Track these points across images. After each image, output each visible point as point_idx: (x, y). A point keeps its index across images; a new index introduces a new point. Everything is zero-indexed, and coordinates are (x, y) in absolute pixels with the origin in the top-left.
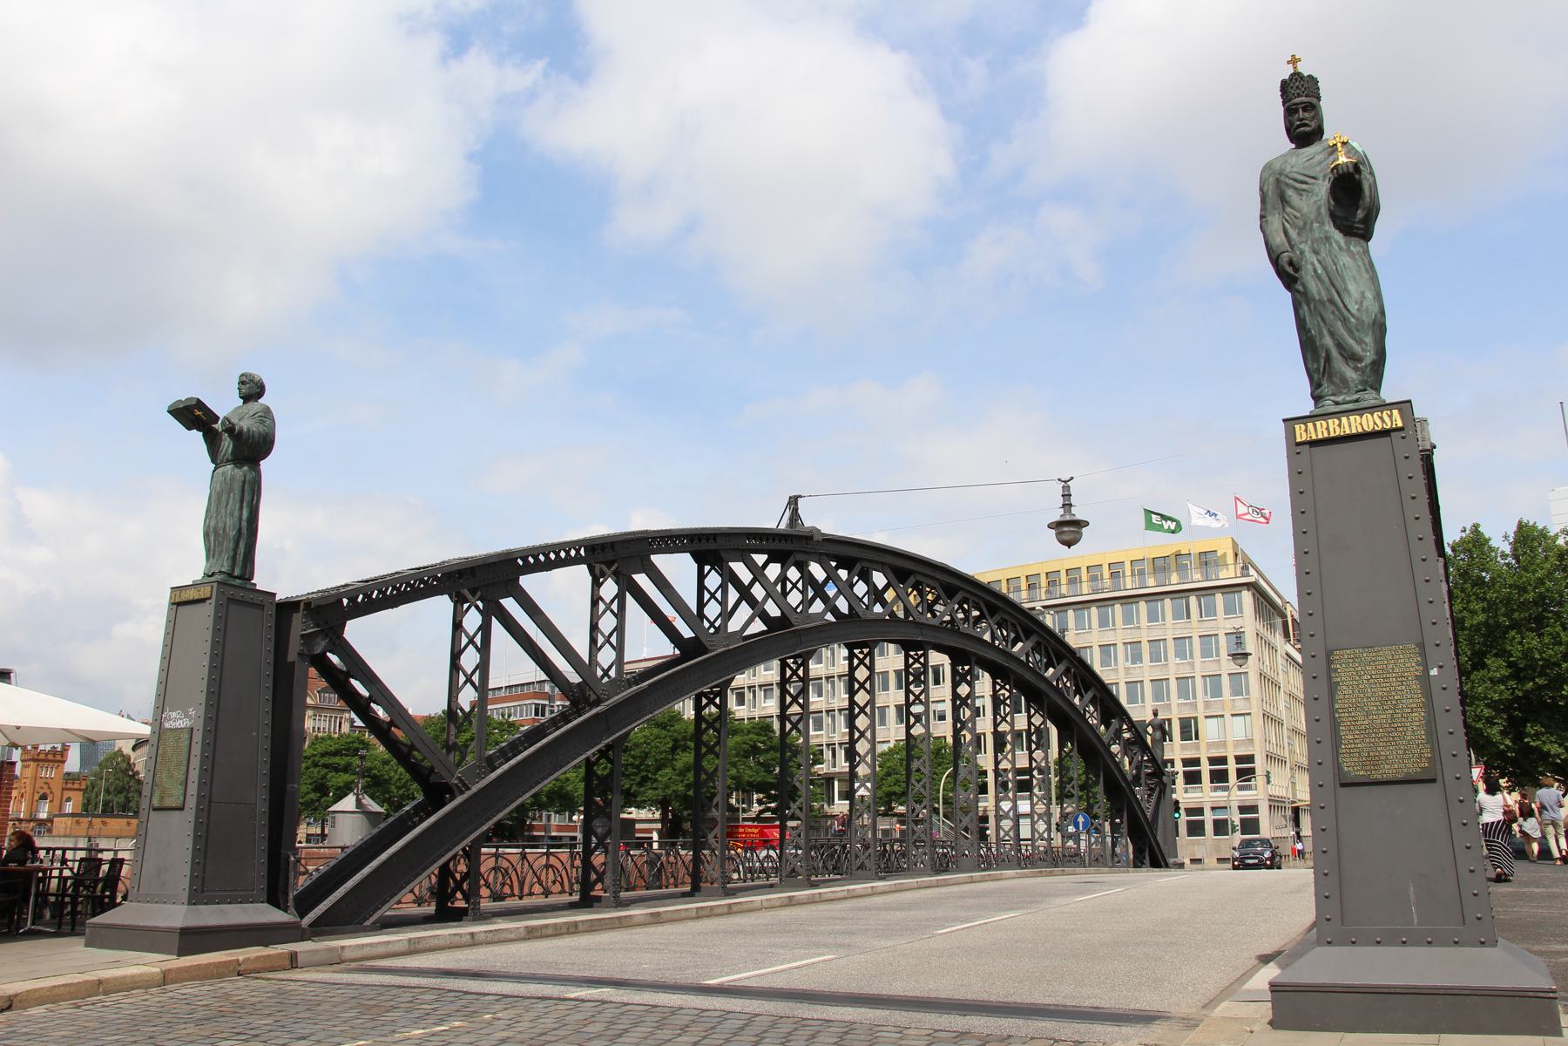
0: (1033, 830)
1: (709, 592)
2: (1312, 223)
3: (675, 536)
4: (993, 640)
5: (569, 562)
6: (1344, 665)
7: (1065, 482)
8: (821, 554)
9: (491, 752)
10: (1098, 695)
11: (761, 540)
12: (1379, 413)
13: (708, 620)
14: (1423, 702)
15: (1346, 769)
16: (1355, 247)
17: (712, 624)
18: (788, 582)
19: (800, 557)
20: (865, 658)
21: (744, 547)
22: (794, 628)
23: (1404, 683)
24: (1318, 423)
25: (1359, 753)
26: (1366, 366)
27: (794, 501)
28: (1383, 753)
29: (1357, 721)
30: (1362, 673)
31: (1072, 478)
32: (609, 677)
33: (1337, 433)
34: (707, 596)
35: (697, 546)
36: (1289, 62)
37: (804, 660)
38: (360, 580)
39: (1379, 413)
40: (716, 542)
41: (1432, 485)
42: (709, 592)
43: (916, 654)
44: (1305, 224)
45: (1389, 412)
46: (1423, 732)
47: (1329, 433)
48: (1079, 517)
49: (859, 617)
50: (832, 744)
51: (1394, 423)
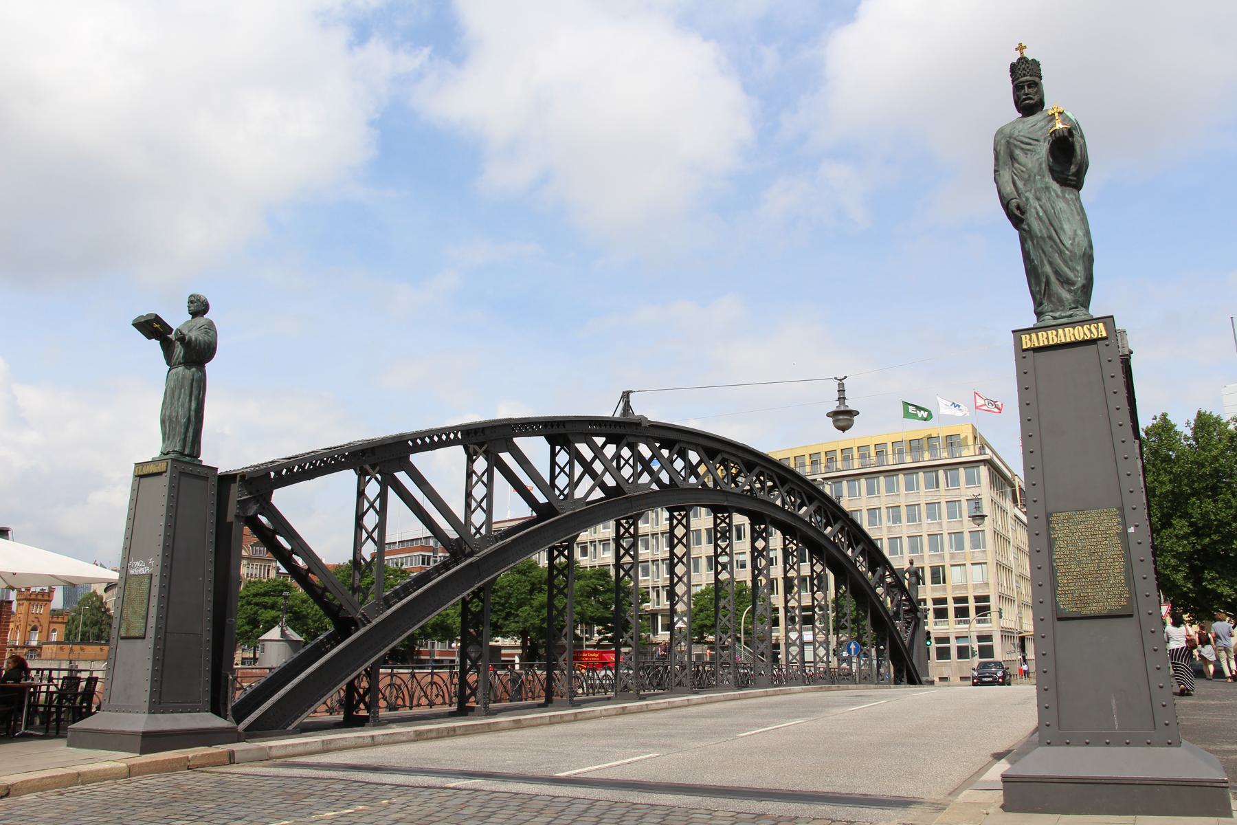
0: (815, 655)
1: (559, 467)
2: (1035, 176)
3: (533, 423)
4: (783, 505)
5: (449, 443)
6: (1060, 525)
7: (840, 380)
8: (647, 437)
9: (387, 593)
10: (866, 548)
11: (600, 426)
12: (1088, 326)
13: (559, 489)
14: (1122, 554)
15: (1062, 606)
16: (1069, 195)
17: (562, 492)
18: (622, 459)
19: (631, 439)
20: (682, 519)
21: (587, 432)
22: (627, 496)
23: (1108, 539)
24: (1040, 334)
25: (1072, 594)
26: (1078, 289)
27: (626, 395)
28: (1091, 594)
29: (1071, 568)
30: (1075, 531)
31: (846, 377)
32: (481, 534)
33: (1055, 342)
34: (558, 470)
35: (550, 431)
37: (634, 521)
38: (284, 457)
39: (1088, 326)
40: (564, 427)
42: (559, 467)
43: (723, 516)
44: (1030, 176)
45: (1095, 325)
46: (1122, 578)
47: (1048, 342)
48: (851, 407)
49: (678, 486)
50: (656, 587)
51: (1100, 334)
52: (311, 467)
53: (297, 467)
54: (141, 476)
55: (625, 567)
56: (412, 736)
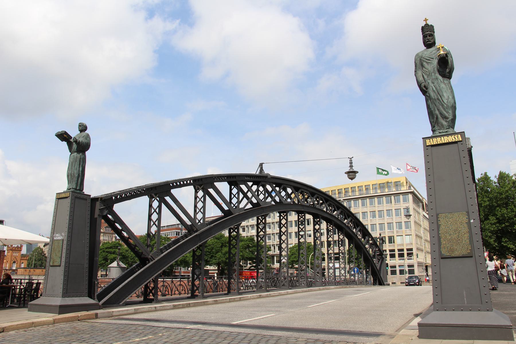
1: (233, 195)
2: (432, 73)
3: (222, 176)
4: (327, 211)
5: (187, 185)
6: (442, 219)
7: (351, 158)
8: (270, 182)
10: (361, 228)
11: (250, 178)
12: (454, 136)
13: (233, 204)
14: (468, 231)
15: (443, 253)
16: (446, 81)
17: (234, 205)
18: (259, 191)
19: (263, 183)
20: (285, 216)
21: (245, 180)
22: (261, 207)
23: (462, 225)
24: (434, 139)
25: (447, 248)
26: (450, 120)
27: (261, 165)
28: (455, 248)
29: (447, 237)
30: (448, 221)
31: (353, 157)
32: (200, 223)
33: (440, 143)
34: (233, 196)
35: (230, 180)
36: (424, 21)
37: (265, 217)
38: (118, 191)
39: (454, 136)
40: (235, 178)
41: (471, 160)
42: (233, 195)
43: (302, 215)
44: (429, 74)
45: (457, 136)
46: (468, 241)
47: (437, 142)
48: (355, 170)
49: (283, 203)
50: (274, 245)
51: (459, 139)
52: (130, 195)
53: (124, 195)
54: (59, 199)
55: (261, 236)
56: (172, 307)
